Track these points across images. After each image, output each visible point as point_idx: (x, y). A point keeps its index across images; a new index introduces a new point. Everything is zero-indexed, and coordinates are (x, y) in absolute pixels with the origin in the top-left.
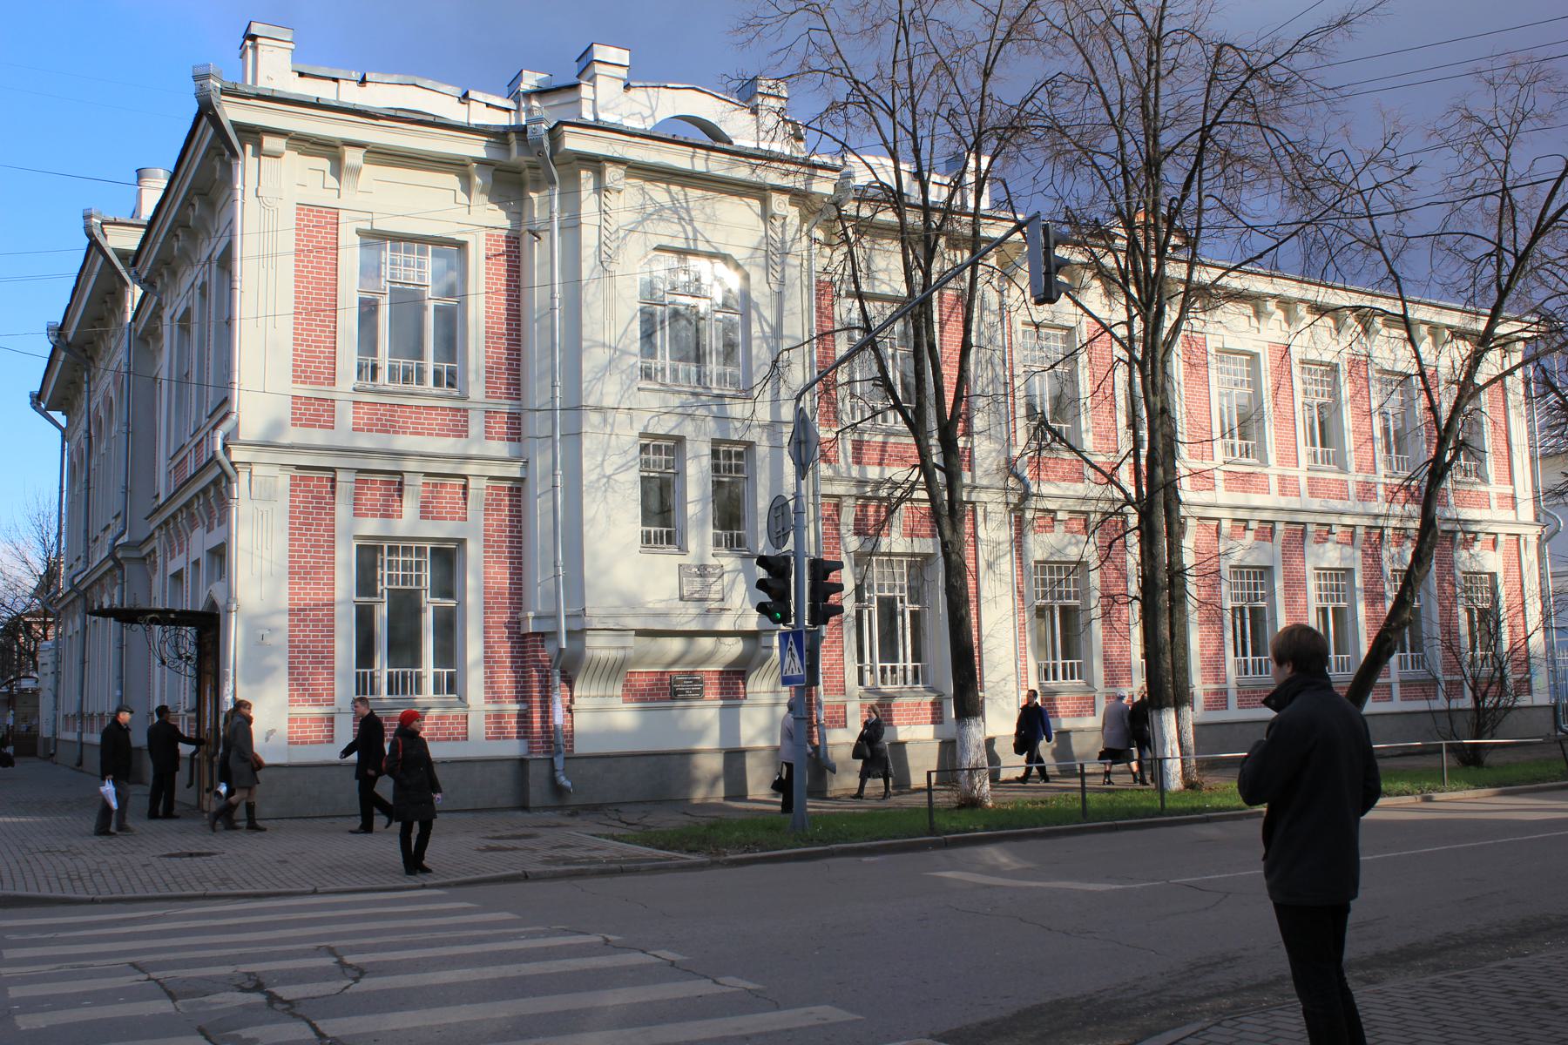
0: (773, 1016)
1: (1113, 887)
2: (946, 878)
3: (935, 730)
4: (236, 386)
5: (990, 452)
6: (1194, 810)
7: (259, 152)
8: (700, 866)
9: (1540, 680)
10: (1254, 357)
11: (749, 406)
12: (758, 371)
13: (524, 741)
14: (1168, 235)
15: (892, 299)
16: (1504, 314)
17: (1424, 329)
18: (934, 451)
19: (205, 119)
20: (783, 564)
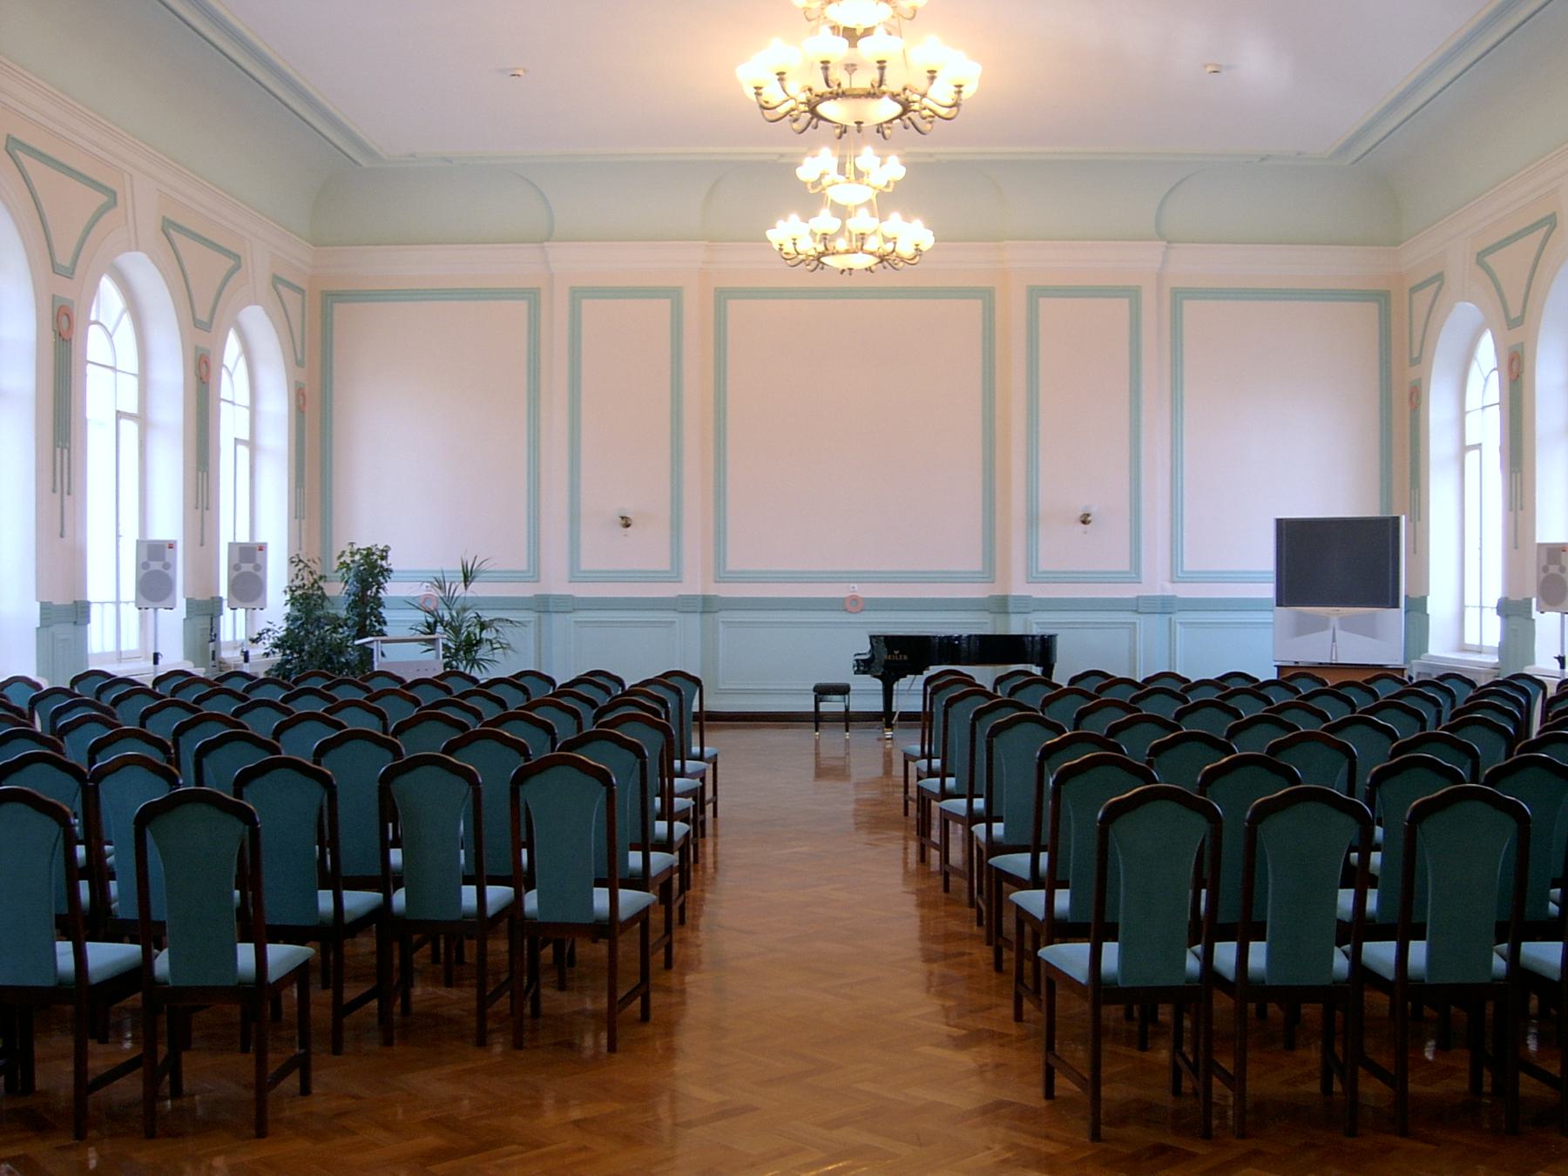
0: (522, 830)
1: (48, 752)
2: (1056, 737)
3: (86, 597)
4: (316, 869)
5: (343, 575)
6: (660, 760)
7: (955, 92)
8: (906, 863)
9: (450, 644)
10: (673, 294)
11: (1393, 619)
12: (676, 902)
13: (957, 96)
14: (34, 736)
15: (813, 256)
16: (1410, 1055)
17: (27, 717)
18: (331, 975)
19: (951, 823)
20: (237, 549)
